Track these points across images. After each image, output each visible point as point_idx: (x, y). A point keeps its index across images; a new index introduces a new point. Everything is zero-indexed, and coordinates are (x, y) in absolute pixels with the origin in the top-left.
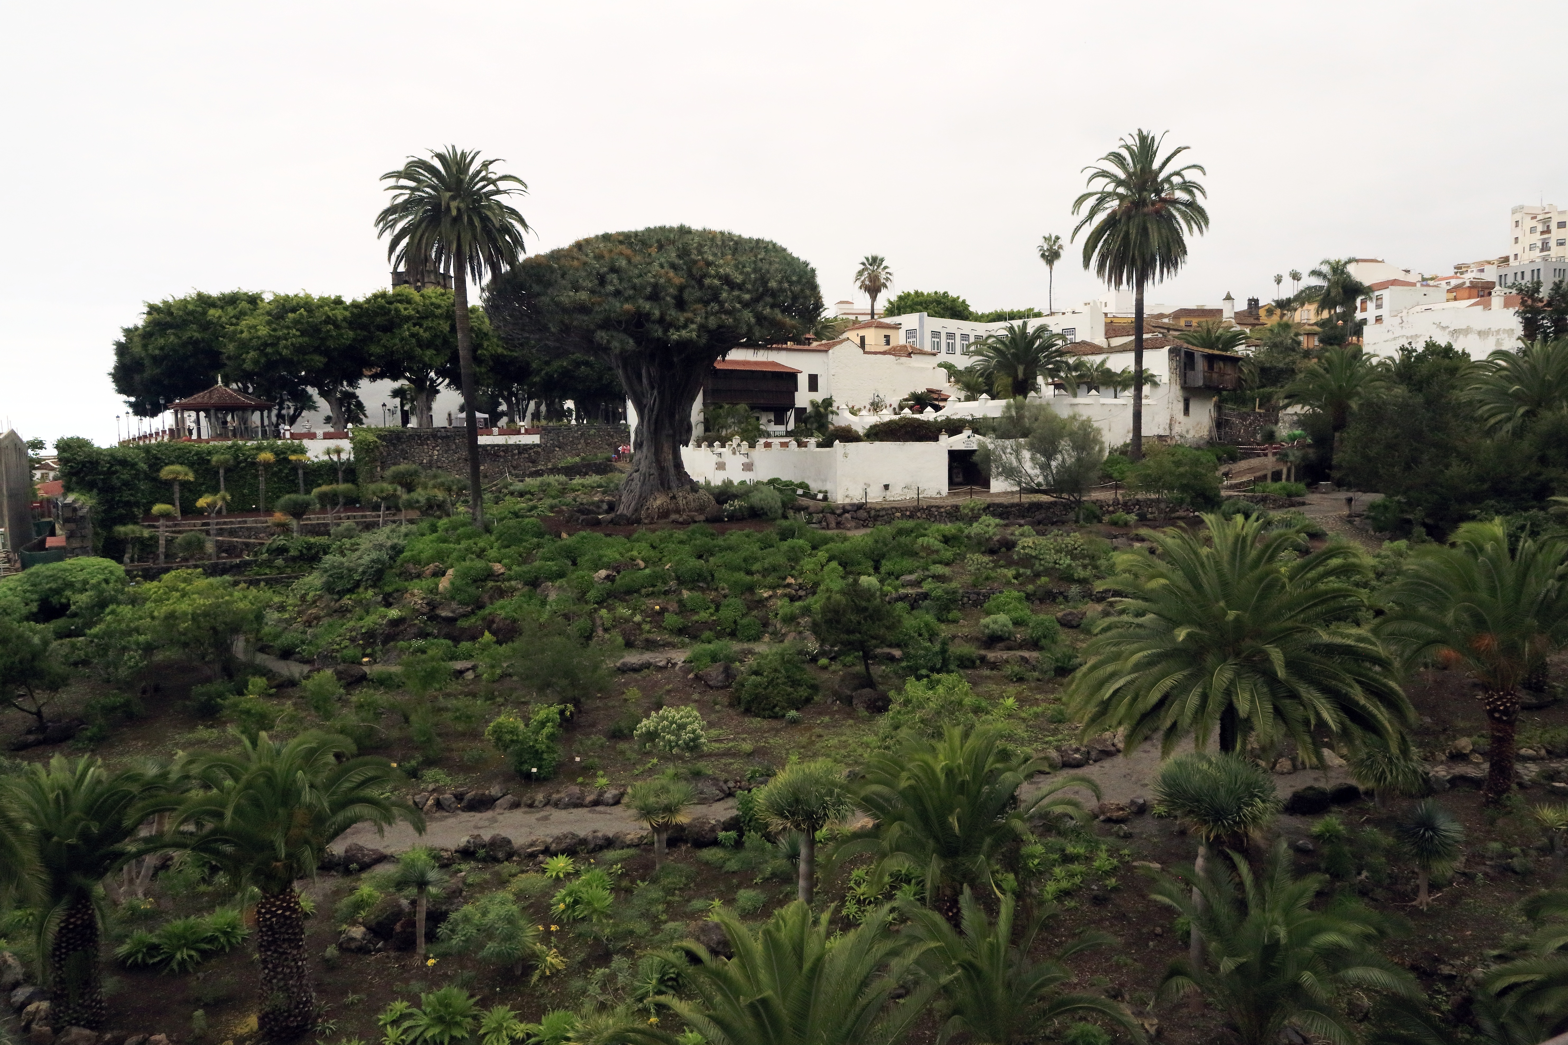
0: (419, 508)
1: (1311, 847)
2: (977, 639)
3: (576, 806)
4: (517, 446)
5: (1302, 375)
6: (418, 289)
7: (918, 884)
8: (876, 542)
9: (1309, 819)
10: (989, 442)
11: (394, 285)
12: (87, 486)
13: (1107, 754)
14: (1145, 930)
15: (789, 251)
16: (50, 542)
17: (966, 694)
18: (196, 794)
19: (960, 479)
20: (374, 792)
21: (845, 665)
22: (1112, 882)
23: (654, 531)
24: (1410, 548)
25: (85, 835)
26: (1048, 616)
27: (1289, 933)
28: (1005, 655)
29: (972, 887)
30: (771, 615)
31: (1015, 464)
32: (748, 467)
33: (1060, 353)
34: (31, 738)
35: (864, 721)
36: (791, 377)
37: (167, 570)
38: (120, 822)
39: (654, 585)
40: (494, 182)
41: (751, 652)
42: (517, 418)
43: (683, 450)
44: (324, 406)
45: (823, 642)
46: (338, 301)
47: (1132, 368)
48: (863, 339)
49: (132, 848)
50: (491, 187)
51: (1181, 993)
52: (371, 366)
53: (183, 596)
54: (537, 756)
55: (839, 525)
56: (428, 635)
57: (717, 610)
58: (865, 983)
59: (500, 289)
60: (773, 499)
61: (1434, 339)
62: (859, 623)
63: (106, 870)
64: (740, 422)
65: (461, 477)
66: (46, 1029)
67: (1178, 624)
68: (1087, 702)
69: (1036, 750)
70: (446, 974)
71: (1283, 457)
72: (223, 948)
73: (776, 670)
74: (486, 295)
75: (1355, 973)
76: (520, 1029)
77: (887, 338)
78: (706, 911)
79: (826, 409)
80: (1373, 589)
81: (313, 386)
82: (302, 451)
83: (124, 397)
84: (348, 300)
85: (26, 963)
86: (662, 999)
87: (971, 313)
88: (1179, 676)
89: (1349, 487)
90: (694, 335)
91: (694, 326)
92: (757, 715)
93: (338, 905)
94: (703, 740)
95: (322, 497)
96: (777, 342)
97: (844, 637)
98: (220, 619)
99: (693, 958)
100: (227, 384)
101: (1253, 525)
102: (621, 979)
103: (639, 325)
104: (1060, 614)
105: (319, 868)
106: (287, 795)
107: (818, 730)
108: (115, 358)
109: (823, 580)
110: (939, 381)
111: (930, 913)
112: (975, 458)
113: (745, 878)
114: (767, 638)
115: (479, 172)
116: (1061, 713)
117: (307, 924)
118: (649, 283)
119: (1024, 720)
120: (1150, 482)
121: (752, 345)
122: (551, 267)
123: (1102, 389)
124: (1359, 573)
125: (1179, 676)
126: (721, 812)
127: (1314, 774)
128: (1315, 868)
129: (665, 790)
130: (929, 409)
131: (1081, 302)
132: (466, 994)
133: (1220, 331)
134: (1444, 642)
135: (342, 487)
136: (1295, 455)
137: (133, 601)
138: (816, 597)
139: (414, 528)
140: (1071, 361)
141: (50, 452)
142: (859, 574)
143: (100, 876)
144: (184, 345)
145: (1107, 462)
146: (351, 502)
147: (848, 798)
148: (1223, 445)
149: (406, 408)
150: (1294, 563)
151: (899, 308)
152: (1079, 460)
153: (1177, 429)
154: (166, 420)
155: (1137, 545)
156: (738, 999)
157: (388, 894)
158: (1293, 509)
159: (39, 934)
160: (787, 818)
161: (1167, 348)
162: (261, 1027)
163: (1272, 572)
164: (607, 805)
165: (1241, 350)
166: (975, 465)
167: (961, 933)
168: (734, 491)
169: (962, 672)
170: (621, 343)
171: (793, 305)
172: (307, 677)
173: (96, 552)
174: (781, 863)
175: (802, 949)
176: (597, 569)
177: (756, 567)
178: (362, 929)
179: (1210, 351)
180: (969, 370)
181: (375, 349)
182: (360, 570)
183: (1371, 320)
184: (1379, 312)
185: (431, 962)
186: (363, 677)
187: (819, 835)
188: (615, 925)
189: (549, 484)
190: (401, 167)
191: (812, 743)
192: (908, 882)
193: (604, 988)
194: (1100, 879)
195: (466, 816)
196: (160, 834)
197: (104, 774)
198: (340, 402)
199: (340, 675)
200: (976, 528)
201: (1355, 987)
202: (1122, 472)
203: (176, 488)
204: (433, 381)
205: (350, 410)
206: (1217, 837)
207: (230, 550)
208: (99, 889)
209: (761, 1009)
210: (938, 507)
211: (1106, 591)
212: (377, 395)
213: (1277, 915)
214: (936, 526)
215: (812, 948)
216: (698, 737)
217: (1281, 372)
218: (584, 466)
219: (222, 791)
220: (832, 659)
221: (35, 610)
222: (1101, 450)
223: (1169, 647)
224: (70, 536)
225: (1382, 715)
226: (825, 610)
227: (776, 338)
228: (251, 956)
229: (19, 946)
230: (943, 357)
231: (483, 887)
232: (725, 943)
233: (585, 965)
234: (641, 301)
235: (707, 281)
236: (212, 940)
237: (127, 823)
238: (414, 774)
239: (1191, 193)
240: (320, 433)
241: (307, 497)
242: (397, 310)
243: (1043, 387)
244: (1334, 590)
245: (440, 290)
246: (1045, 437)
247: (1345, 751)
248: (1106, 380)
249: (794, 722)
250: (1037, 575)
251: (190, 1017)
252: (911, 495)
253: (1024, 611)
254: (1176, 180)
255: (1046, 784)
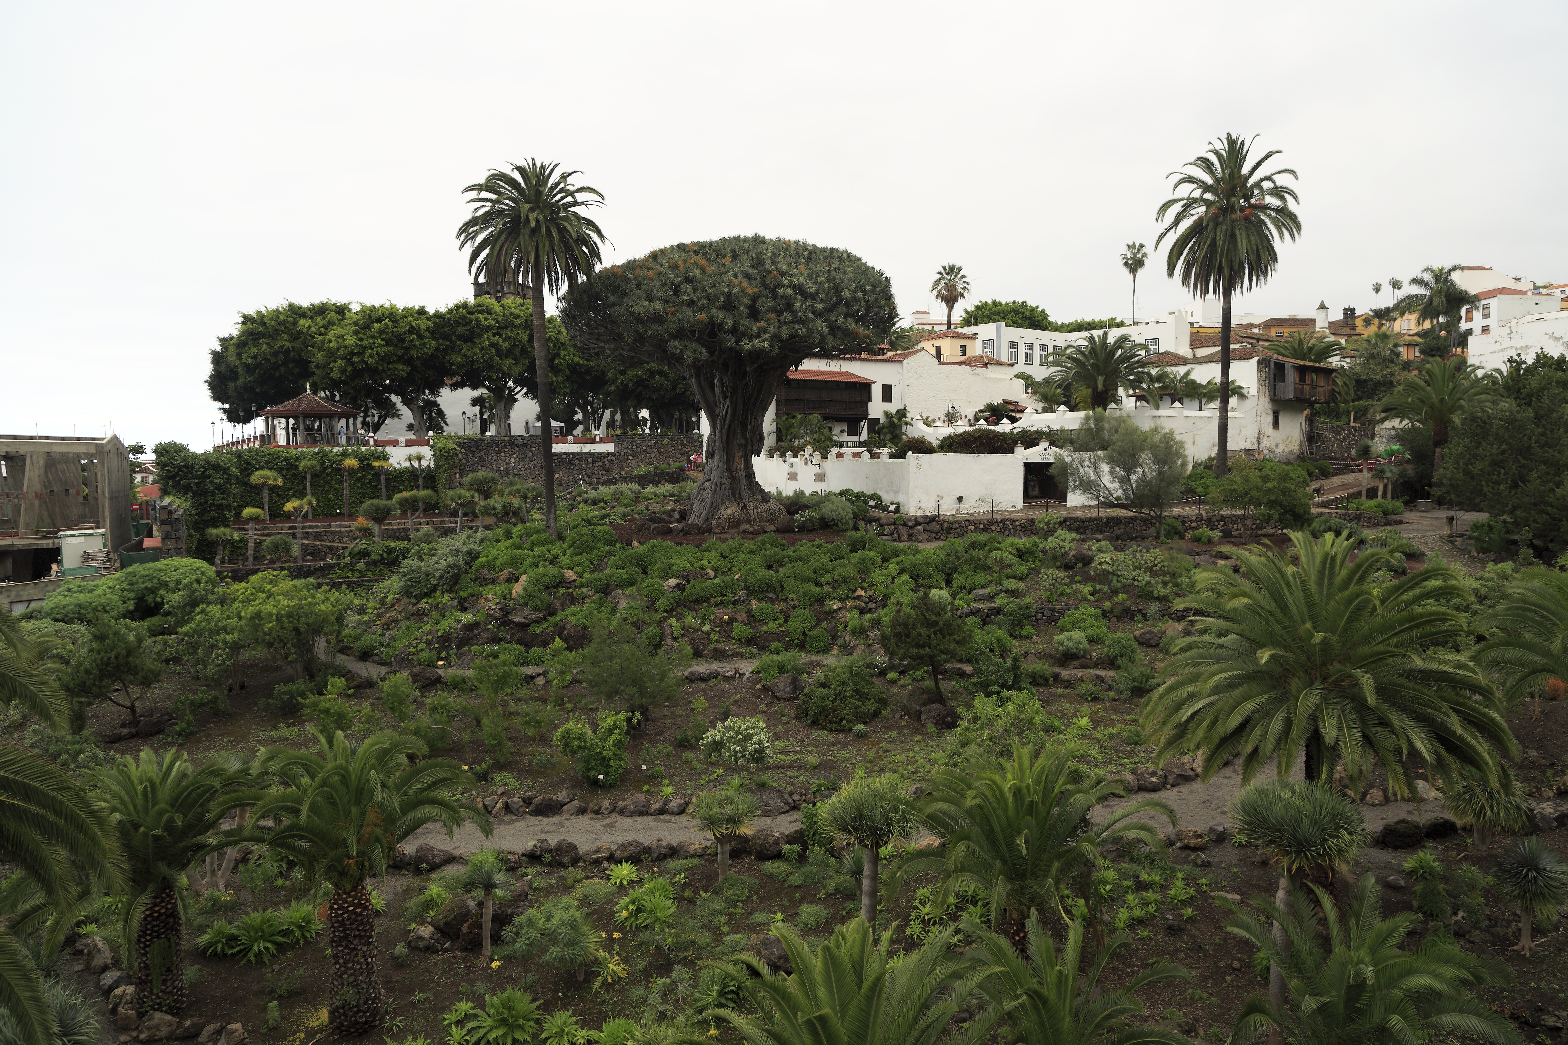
0: (495, 515)
1: (1402, 883)
2: (1050, 656)
3: (642, 814)
4: (592, 455)
5: (1401, 388)
6: (498, 299)
7: (984, 906)
8: (949, 555)
9: (1400, 854)
10: (1067, 455)
11: (475, 296)
12: (182, 490)
13: (1185, 779)
14: (1222, 964)
15: (864, 260)
16: (148, 543)
17: (1037, 712)
18: (275, 790)
19: (1036, 493)
20: (444, 794)
21: (914, 680)
22: (1189, 912)
23: (724, 541)
24: (1516, 571)
25: (170, 827)
26: (1124, 634)
27: (1377, 973)
28: (1080, 673)
29: (1039, 911)
30: (841, 627)
31: (1093, 477)
32: (820, 478)
33: (1143, 364)
34: (125, 731)
35: (931, 737)
36: (865, 387)
37: (255, 572)
38: (202, 815)
39: (722, 596)
40: (572, 194)
41: (819, 664)
42: (592, 427)
43: (755, 460)
44: (407, 414)
45: (892, 655)
46: (422, 312)
47: (1218, 380)
48: (938, 349)
49: (213, 841)
50: (569, 199)
51: (1260, 1032)
52: (452, 375)
53: (268, 597)
54: (604, 763)
55: (911, 537)
56: (501, 640)
57: (786, 621)
58: (926, 1006)
59: (577, 301)
60: (845, 510)
61: (1546, 350)
62: (929, 637)
63: (189, 862)
64: (813, 433)
65: (537, 485)
66: (131, 1012)
67: (1262, 646)
68: (1164, 723)
69: (1111, 772)
70: (510, 977)
71: (1379, 474)
72: (298, 940)
73: (844, 683)
74: (563, 305)
75: (1449, 1019)
76: (582, 1034)
77: (963, 347)
78: (766, 925)
79: (900, 419)
80: (1475, 613)
81: (397, 394)
82: (385, 457)
83: (219, 404)
84: (431, 311)
85: (114, 949)
86: (720, 1012)
87: (1050, 323)
88: (1261, 699)
89: (1451, 505)
90: (767, 344)
91: (767, 336)
92: (824, 728)
93: (408, 904)
94: (768, 752)
95: (403, 503)
96: (851, 353)
97: (914, 651)
98: (303, 620)
99: (754, 972)
100: (315, 392)
101: (1343, 543)
102: (681, 990)
103: (713, 334)
104: (1138, 633)
105: (389, 866)
106: (361, 794)
107: (885, 745)
108: (211, 366)
109: (893, 592)
110: (1016, 392)
111: (994, 936)
112: (1052, 471)
113: (808, 892)
114: (835, 650)
115: (558, 184)
116: (1138, 735)
117: (377, 921)
118: (723, 293)
119: (1098, 741)
120: (1235, 498)
121: (825, 355)
122: (626, 277)
123: (1186, 401)
124: (1458, 596)
125: (1261, 699)
126: (786, 825)
127: (1410, 806)
128: (1407, 907)
129: (729, 800)
130: (1005, 420)
131: (1166, 312)
132: (528, 997)
133: (1313, 341)
134: (1551, 671)
135: (423, 493)
136: (1392, 472)
137: (222, 602)
138: (886, 610)
139: (489, 534)
140: (1154, 372)
141: (149, 457)
142: (930, 587)
143: (184, 866)
144: (275, 354)
145: (1190, 476)
146: (431, 508)
147: (914, 815)
148: (1316, 460)
149: (485, 416)
150: (1389, 584)
151: (976, 318)
152: (1160, 473)
153: (1265, 443)
154: (258, 426)
155: (1222, 562)
156: (795, 1015)
157: (456, 895)
158: (1389, 528)
159: (126, 921)
160: (850, 833)
161: (1256, 359)
162: (331, 1021)
163: (1361, 593)
164: (672, 814)
165: (1335, 361)
166: (1051, 478)
167: (1027, 958)
168: (805, 501)
169: (1034, 690)
170: (694, 352)
171: (867, 314)
172: (383, 679)
173: (190, 553)
174: (845, 879)
175: (862, 968)
176: (666, 577)
177: (824, 579)
178: (431, 928)
179: (1302, 363)
180: (1048, 381)
181: (457, 359)
182: (437, 574)
183: (1477, 330)
184: (1486, 322)
185: (495, 964)
186: (438, 680)
187: (884, 851)
188: (677, 935)
189: (622, 493)
190: (482, 181)
191: (879, 758)
192: (975, 904)
193: (664, 997)
194: (1176, 908)
195: (533, 820)
196: (241, 828)
197: (190, 768)
198: (422, 410)
199: (415, 677)
200: (1051, 543)
201: (1448, 1034)
202: (1206, 487)
203: (266, 493)
204: (511, 390)
205: (431, 418)
206: (1300, 869)
207: (315, 553)
208: (183, 880)
209: (819, 1027)
210: (1013, 521)
211: (1187, 610)
212: (457, 403)
213: (1363, 953)
214: (1008, 541)
215: (872, 968)
216: (764, 749)
217: (1379, 384)
218: (657, 475)
219: (298, 788)
220: (901, 673)
221: (131, 608)
222: (1184, 464)
223: (1251, 668)
224: (166, 537)
225: (1481, 746)
226: (894, 624)
227: (851, 348)
228: (324, 950)
229: (107, 931)
230: (1020, 368)
231: (548, 891)
232: (785, 958)
233: (647, 974)
234: (714, 311)
235: (781, 291)
236: (286, 933)
237: (209, 816)
238: (483, 777)
239: (1282, 198)
240: (402, 440)
241: (388, 503)
242: (478, 320)
243: (1124, 399)
244: (1431, 614)
245: (519, 300)
246: (1125, 449)
247: (1441, 784)
248: (1190, 392)
249: (861, 736)
250: (1115, 592)
251: (265, 1009)
252: (986, 507)
253: (1101, 628)
254: (1267, 185)
255: (1120, 808)
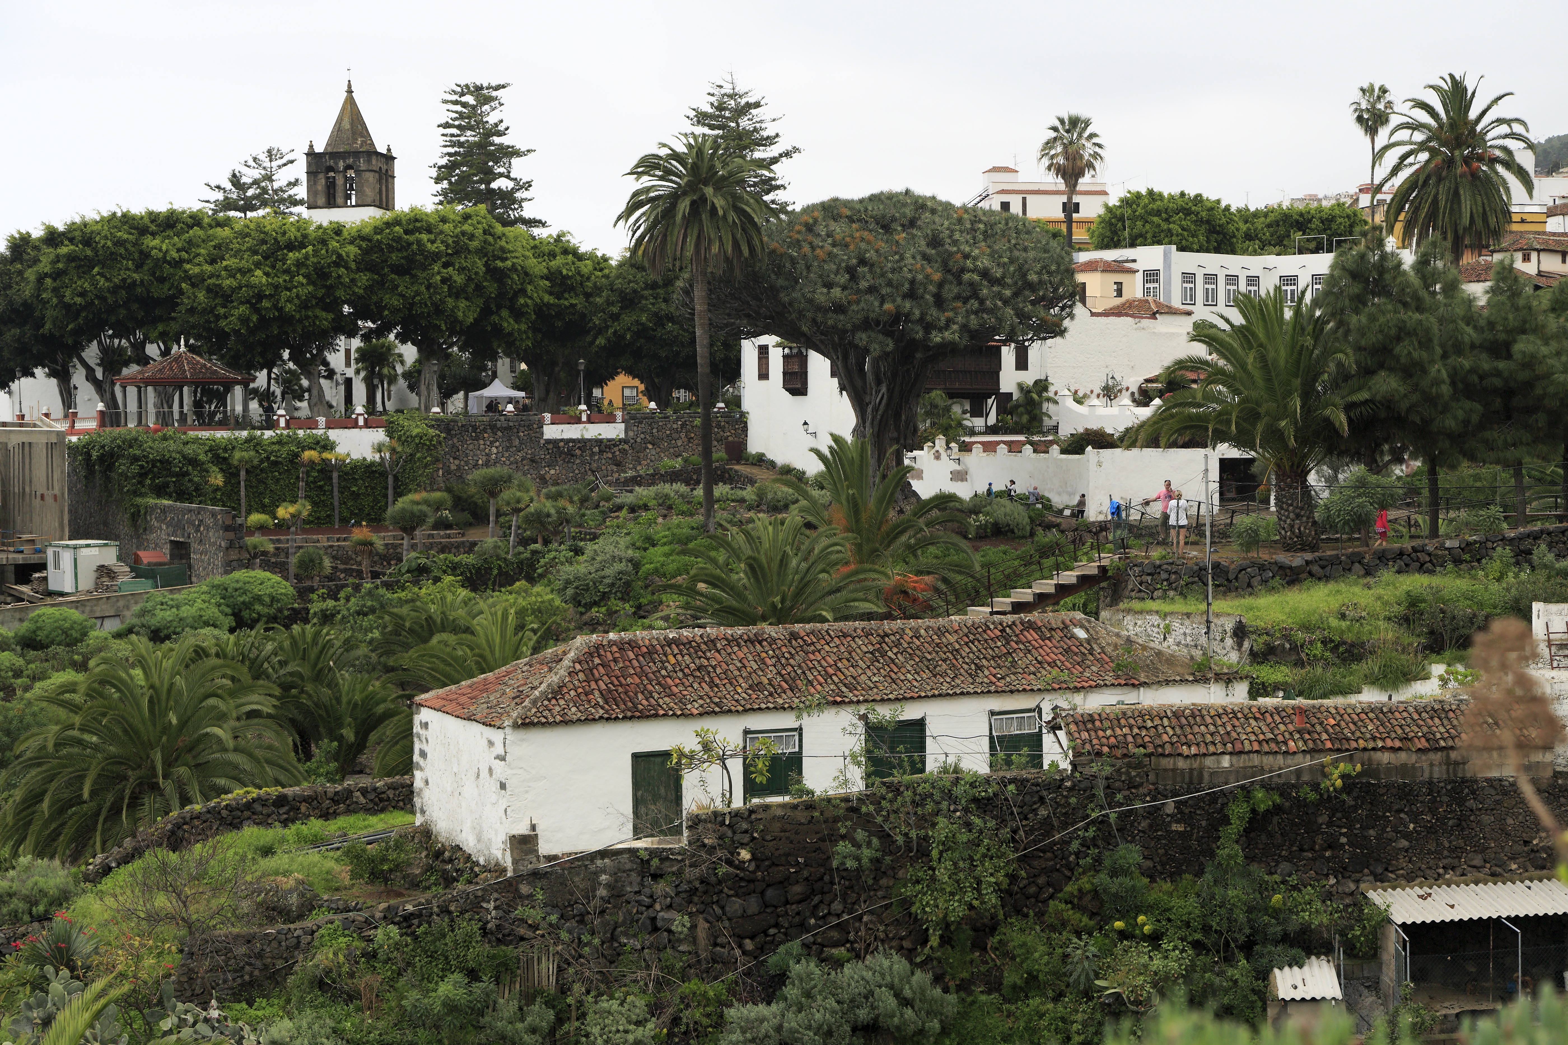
4: (599, 442)
32: (959, 476)
60: (1019, 515)
77: (1119, 284)
91: (955, 327)
144: (115, 290)
230: (1202, 313)
235: (967, 276)
242: (419, 242)
